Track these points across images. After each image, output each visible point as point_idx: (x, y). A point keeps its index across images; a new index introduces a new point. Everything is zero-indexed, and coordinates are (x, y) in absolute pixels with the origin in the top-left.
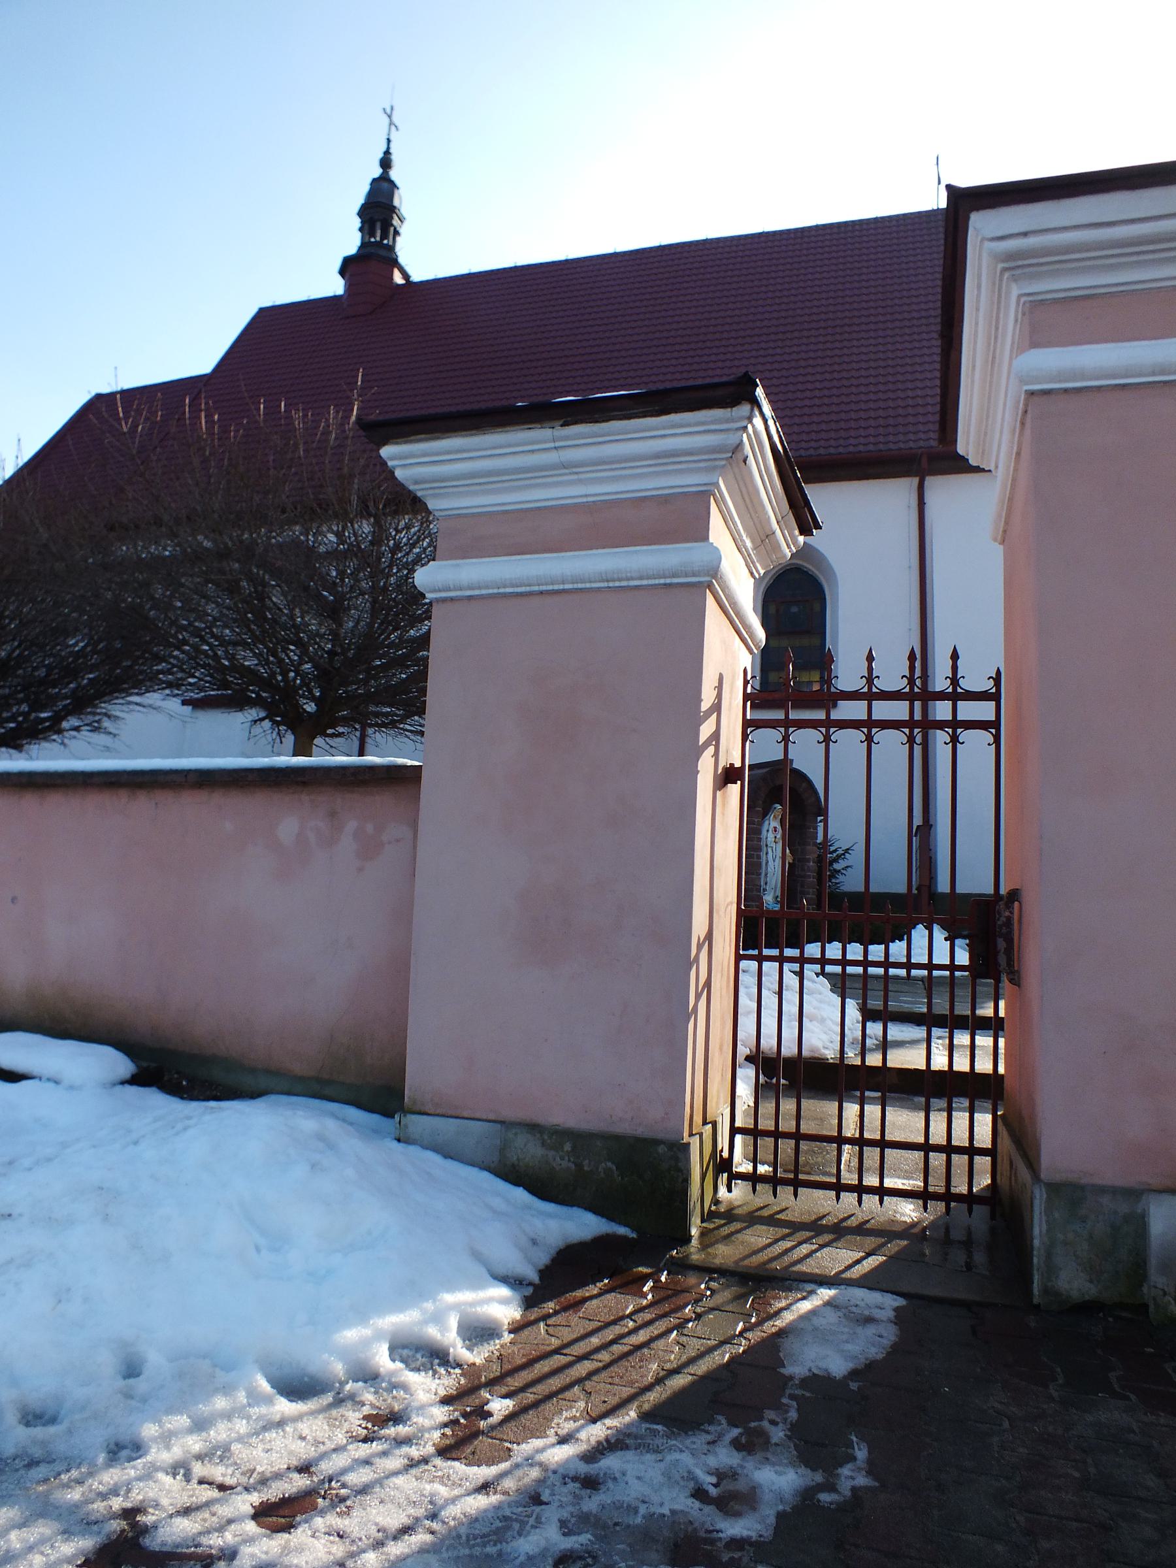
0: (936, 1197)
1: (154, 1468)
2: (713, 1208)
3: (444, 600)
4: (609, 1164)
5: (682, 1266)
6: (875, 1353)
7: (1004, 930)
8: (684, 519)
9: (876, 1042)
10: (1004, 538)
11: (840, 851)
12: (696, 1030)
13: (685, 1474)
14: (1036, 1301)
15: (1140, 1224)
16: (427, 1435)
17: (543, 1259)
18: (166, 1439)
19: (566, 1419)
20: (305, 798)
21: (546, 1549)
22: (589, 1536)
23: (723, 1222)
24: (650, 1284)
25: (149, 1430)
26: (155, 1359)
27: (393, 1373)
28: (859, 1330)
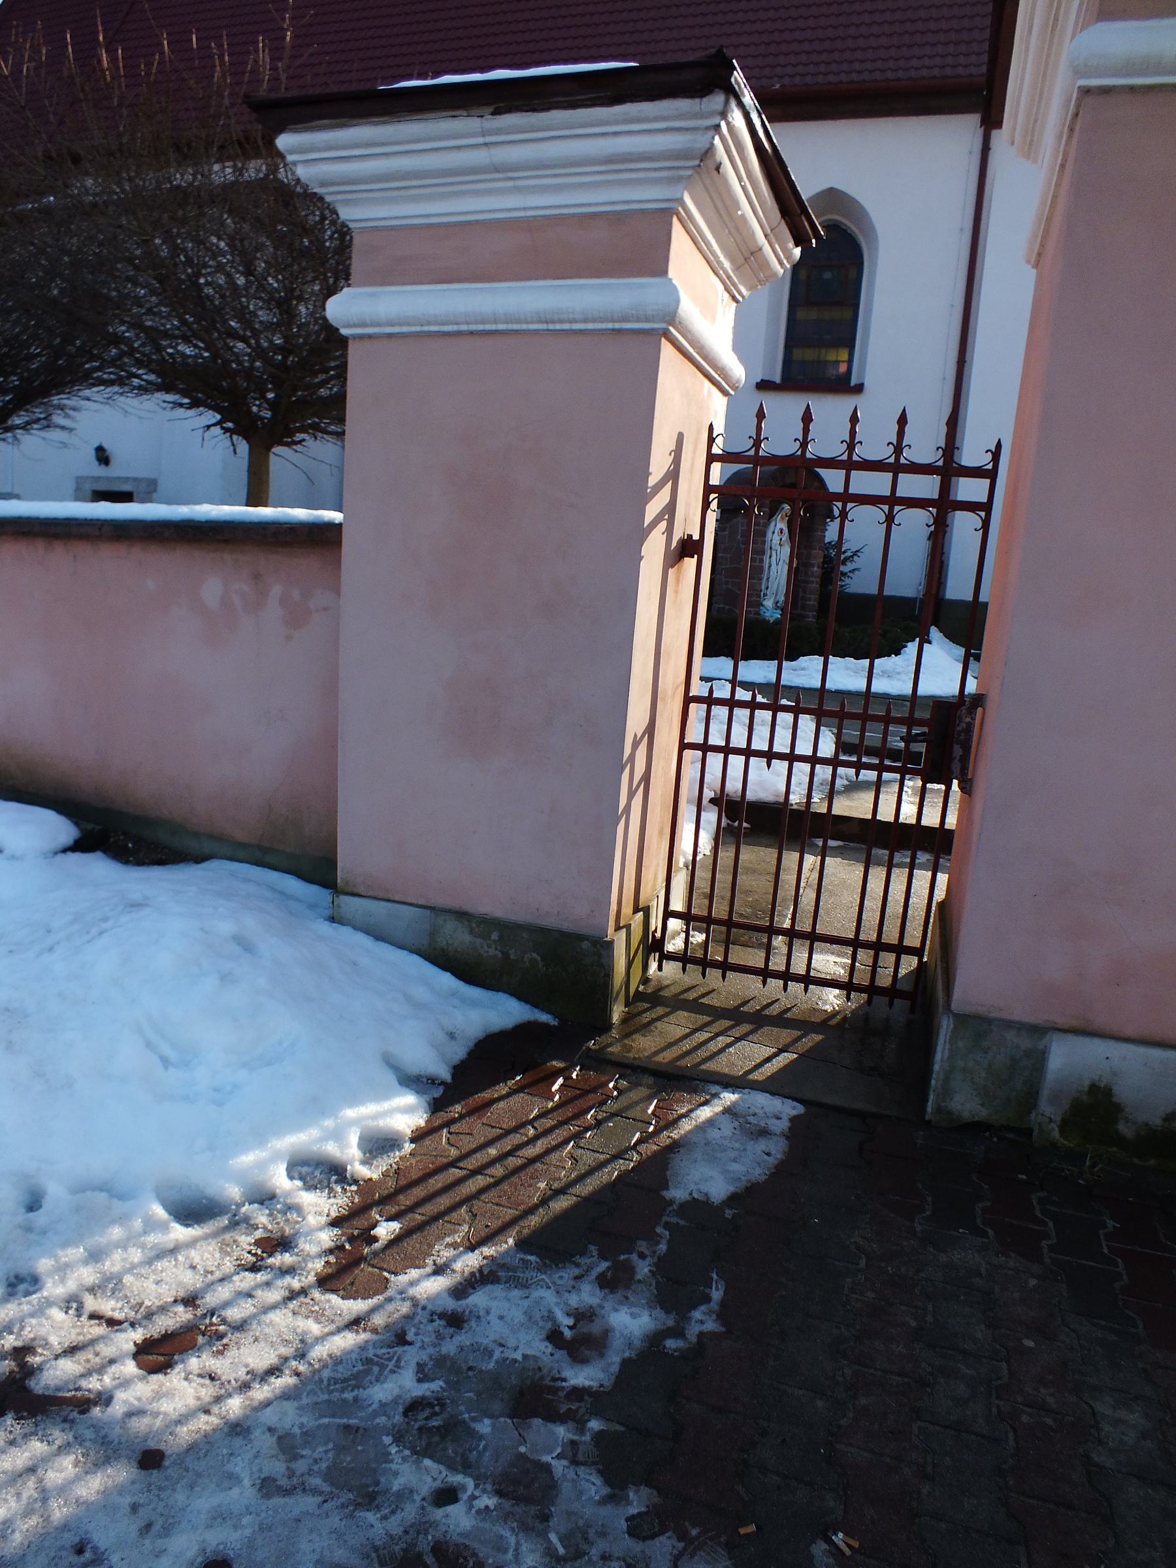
0: (860, 989)
1: (49, 1303)
2: (641, 988)
3: (361, 337)
4: (535, 955)
5: (599, 1062)
6: (758, 1174)
7: (962, 737)
8: (637, 246)
9: (846, 783)
10: (1038, 261)
11: (849, 554)
12: (626, 836)
13: (546, 1314)
14: (927, 1117)
15: (1040, 1059)
16: (310, 1265)
17: (459, 1052)
18: (63, 1270)
19: (448, 1245)
20: (227, 557)
21: (399, 1397)
22: (441, 1383)
23: (647, 1005)
24: (560, 1081)
25: (44, 1265)
26: (56, 1192)
27: (288, 1194)
28: (750, 1145)
